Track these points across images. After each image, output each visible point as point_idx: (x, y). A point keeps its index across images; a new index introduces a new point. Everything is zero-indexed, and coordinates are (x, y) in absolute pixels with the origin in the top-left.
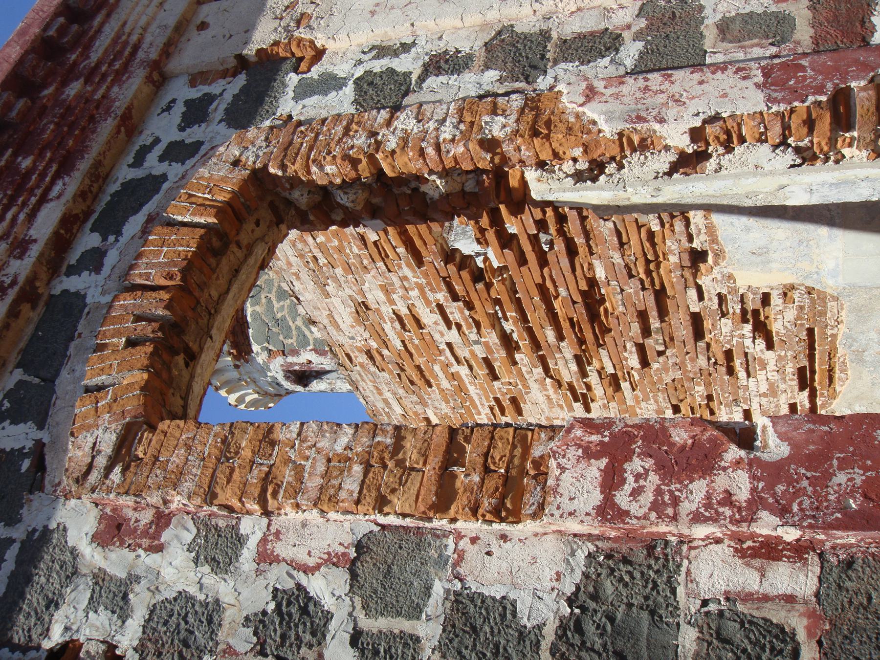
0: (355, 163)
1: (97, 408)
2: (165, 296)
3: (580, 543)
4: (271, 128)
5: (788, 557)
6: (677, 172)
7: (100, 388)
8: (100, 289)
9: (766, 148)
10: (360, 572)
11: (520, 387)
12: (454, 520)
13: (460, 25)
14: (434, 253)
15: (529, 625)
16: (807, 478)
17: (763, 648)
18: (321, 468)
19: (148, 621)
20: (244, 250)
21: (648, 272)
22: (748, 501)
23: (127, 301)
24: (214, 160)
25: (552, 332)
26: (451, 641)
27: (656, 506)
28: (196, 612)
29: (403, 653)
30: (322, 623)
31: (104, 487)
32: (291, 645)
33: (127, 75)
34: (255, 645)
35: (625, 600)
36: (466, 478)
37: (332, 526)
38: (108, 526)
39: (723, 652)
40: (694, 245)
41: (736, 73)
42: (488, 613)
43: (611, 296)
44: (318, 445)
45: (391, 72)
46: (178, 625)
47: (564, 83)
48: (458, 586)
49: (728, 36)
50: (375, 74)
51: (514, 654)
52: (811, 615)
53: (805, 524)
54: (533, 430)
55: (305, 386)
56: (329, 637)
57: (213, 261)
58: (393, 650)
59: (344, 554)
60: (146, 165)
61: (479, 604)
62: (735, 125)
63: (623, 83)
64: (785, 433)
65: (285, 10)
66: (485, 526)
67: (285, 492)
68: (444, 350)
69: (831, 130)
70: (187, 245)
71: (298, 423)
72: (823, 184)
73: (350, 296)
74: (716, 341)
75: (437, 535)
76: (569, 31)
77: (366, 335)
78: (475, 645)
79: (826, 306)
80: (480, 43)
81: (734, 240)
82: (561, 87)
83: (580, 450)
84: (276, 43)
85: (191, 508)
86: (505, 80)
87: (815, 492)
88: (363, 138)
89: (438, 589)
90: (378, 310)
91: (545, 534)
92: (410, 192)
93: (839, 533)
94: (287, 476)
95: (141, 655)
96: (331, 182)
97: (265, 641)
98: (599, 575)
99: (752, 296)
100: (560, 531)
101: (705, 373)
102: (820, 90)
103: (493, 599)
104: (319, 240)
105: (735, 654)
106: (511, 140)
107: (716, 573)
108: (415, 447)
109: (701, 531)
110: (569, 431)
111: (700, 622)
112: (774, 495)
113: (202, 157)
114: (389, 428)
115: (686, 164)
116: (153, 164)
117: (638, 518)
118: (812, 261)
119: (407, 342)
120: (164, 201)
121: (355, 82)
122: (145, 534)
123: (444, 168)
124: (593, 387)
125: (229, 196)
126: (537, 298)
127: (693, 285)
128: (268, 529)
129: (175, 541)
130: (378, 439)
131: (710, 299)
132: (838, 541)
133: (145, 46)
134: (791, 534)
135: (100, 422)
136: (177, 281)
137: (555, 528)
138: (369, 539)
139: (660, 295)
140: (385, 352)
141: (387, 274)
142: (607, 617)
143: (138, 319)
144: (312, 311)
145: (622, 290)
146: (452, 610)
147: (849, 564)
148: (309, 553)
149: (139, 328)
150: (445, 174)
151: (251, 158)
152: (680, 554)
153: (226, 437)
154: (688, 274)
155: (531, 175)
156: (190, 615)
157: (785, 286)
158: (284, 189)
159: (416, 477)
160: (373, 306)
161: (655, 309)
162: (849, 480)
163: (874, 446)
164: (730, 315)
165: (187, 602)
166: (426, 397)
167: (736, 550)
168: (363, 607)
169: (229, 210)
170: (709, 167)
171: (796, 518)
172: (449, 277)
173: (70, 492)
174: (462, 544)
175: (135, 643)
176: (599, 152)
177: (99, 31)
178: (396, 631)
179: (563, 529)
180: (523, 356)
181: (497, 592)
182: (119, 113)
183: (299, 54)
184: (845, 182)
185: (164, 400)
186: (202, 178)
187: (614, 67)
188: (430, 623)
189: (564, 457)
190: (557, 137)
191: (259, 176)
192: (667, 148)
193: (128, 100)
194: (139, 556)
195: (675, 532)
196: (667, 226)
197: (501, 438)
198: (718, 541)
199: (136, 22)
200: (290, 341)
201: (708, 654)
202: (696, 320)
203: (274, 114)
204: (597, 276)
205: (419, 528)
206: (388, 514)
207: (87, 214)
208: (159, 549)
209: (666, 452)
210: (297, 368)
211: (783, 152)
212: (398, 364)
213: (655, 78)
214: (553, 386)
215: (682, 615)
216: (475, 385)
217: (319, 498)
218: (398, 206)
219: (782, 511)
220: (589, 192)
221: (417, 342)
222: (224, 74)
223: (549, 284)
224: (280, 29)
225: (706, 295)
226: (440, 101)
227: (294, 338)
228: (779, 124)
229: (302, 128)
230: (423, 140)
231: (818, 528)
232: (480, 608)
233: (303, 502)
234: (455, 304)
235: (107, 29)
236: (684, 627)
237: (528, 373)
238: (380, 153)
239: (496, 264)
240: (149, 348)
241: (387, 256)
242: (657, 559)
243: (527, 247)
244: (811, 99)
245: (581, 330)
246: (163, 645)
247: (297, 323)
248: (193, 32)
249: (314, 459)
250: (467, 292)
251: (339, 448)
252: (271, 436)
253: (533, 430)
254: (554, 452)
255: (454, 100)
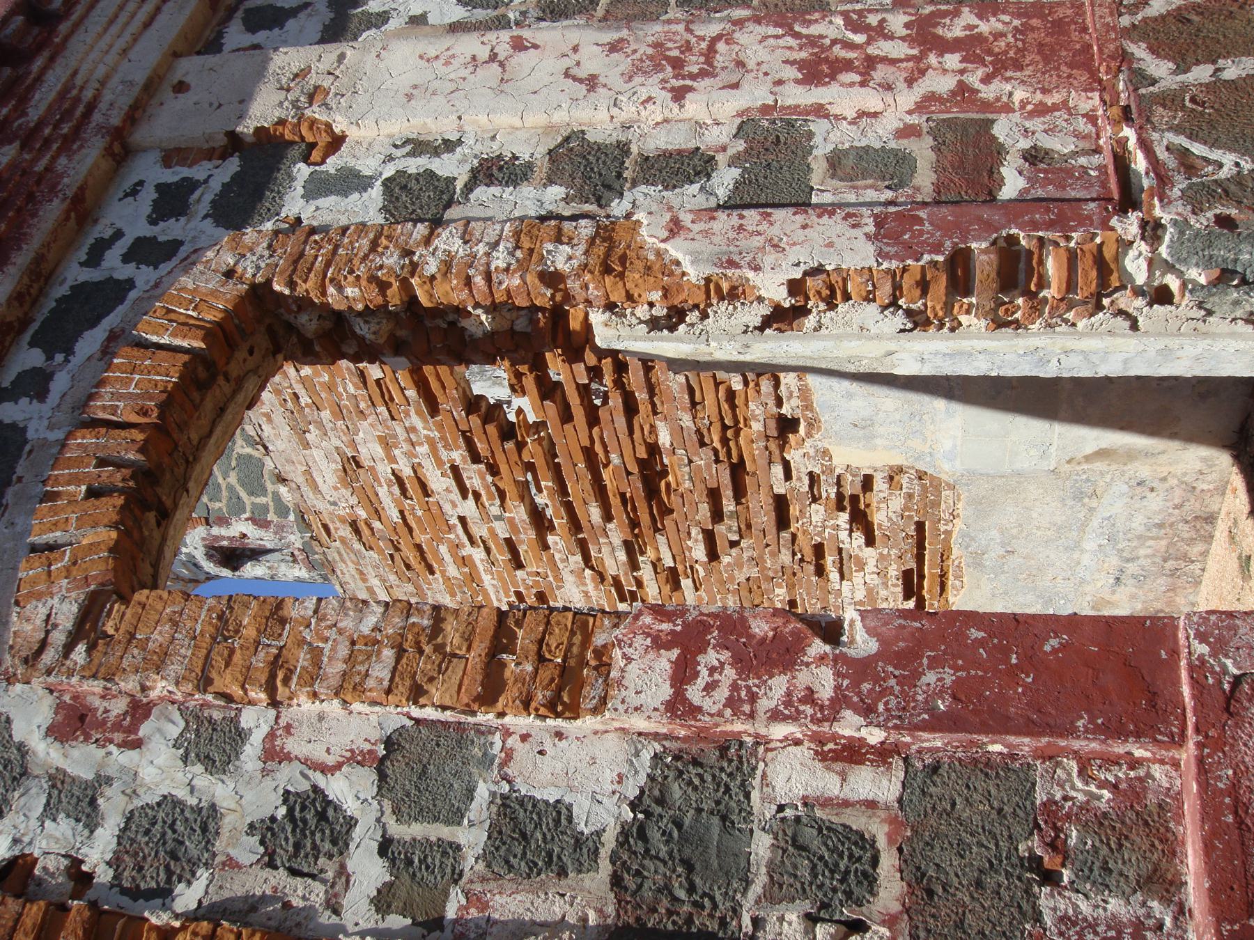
0: (383, 286)
1: (49, 572)
2: (140, 437)
3: (646, 743)
4: (276, 233)
5: (872, 761)
6: (770, 327)
7: (51, 547)
8: (46, 423)
9: (873, 309)
10: (389, 772)
11: (551, 579)
12: (501, 715)
13: (518, 123)
14: (454, 399)
15: (586, 832)
16: (895, 677)
17: (841, 856)
18: (343, 651)
19: (123, 830)
20: (232, 383)
21: (725, 441)
22: (831, 700)
23: (86, 439)
24: (200, 267)
25: (598, 510)
26: (497, 849)
27: (731, 702)
28: (187, 820)
29: (442, 863)
30: (344, 830)
31: (64, 669)
32: (306, 856)
33: (79, 143)
34: (262, 856)
35: (694, 805)
36: (516, 666)
37: (355, 720)
38: (67, 717)
39: (799, 860)
40: (783, 411)
41: (845, 219)
42: (540, 818)
43: (676, 468)
44: (339, 625)
45: (430, 175)
46: (164, 834)
47: (644, 211)
48: (506, 788)
49: (839, 172)
50: (410, 175)
51: (569, 863)
52: (893, 821)
53: (890, 724)
54: (595, 616)
55: (235, 569)
56: (352, 846)
57: (196, 396)
58: (429, 860)
59: (370, 752)
60: (105, 264)
61: (530, 808)
62: (840, 280)
63: (714, 218)
64: (875, 628)
65: (293, 80)
66: (538, 722)
67: (299, 678)
68: (455, 526)
69: (946, 295)
70: (168, 374)
71: (315, 599)
72: (937, 353)
73: (337, 448)
74: (804, 532)
75: (480, 730)
76: (652, 147)
77: (354, 500)
78: (524, 854)
79: (939, 495)
80: (541, 150)
81: (832, 408)
82: (640, 216)
83: (649, 640)
84: (282, 122)
85: (179, 696)
86: (573, 201)
87: (902, 691)
88: (395, 257)
89: (482, 791)
90: (372, 469)
91: (606, 732)
92: (445, 326)
93: (925, 735)
94: (302, 659)
95: (116, 871)
96: (350, 308)
97: (274, 851)
98: (666, 777)
99: (850, 478)
100: (623, 729)
101: (788, 572)
102: (937, 249)
103: (546, 803)
104: (303, 373)
105: (811, 861)
106: (578, 276)
107: (794, 777)
108: (457, 630)
109: (779, 731)
110: (636, 618)
111: (775, 828)
112: (859, 694)
113: (182, 261)
114: (426, 608)
115: (782, 318)
116: (114, 264)
117: (712, 715)
118: (925, 440)
119: (406, 513)
120: (131, 315)
121: (384, 184)
122: (117, 726)
123: (493, 301)
124: (645, 583)
125: (220, 315)
126: (581, 465)
127: (778, 459)
128: (276, 722)
129: (158, 736)
130: (413, 620)
131: (799, 479)
132: (925, 745)
133: (103, 106)
134: (874, 736)
135: (55, 590)
136: (153, 417)
137: (617, 725)
138: (400, 734)
139: (738, 470)
140: (377, 525)
141: (390, 423)
142: (674, 822)
143: (102, 463)
144: (283, 465)
145: (690, 461)
146: (499, 815)
147: (935, 769)
148: (328, 750)
149: (104, 475)
150: (493, 308)
151: (249, 269)
152: (756, 756)
153: (224, 613)
154: (773, 446)
155: (597, 318)
156: (178, 823)
157: (891, 468)
158: (289, 311)
159: (458, 666)
160: (366, 463)
161: (730, 487)
162: (938, 680)
163: (966, 645)
164: (823, 501)
165: (174, 808)
166: (425, 587)
167: (816, 753)
168: (394, 812)
169: (220, 334)
170: (807, 325)
171: (881, 719)
172: (470, 431)
173: (15, 675)
174: (510, 742)
175: (108, 856)
176: (681, 298)
177: (39, 79)
178: (433, 839)
179: (627, 726)
180: (557, 538)
181: (551, 795)
182: (70, 193)
183: (310, 138)
184: (961, 353)
185: (135, 566)
186: (183, 289)
187: (704, 197)
188: (473, 829)
189: (630, 646)
190: (633, 276)
191: (259, 294)
192: (760, 299)
193: (81, 177)
194: (110, 753)
195: (751, 731)
196: (752, 385)
197: (558, 623)
198: (797, 743)
199: (92, 72)
200: (217, 505)
201: (783, 862)
202: (781, 505)
203: (278, 214)
204: (660, 442)
205: (460, 723)
206: (424, 706)
207: (24, 323)
208: (137, 744)
209: (744, 644)
210: (225, 543)
211: (893, 314)
212: (392, 541)
213: (752, 215)
214: (593, 580)
215: (756, 821)
216: (492, 574)
217: (341, 686)
218: (429, 340)
219: (867, 711)
220: (665, 344)
221: (420, 513)
222: (209, 154)
223: (598, 448)
224: (286, 103)
225: (794, 473)
226: (490, 219)
227: (224, 501)
228: (889, 283)
229: (317, 237)
230: (470, 266)
231: (904, 729)
232: (531, 813)
233: (322, 690)
234: (475, 466)
235: (50, 77)
236: (757, 833)
237: (563, 561)
238: (416, 278)
239: (531, 418)
240: (120, 501)
241: (392, 399)
242: (730, 761)
243: (574, 400)
244: (926, 257)
245: (634, 509)
246: (144, 858)
247: (229, 480)
248: (167, 93)
249: (334, 640)
250: (492, 452)
251: (366, 628)
252: (280, 613)
253: (595, 616)
254: (619, 641)
255: (509, 220)
